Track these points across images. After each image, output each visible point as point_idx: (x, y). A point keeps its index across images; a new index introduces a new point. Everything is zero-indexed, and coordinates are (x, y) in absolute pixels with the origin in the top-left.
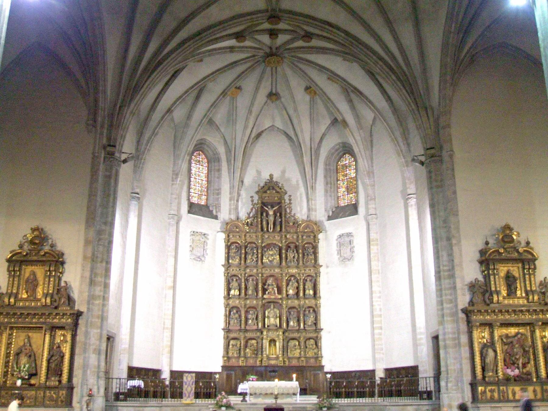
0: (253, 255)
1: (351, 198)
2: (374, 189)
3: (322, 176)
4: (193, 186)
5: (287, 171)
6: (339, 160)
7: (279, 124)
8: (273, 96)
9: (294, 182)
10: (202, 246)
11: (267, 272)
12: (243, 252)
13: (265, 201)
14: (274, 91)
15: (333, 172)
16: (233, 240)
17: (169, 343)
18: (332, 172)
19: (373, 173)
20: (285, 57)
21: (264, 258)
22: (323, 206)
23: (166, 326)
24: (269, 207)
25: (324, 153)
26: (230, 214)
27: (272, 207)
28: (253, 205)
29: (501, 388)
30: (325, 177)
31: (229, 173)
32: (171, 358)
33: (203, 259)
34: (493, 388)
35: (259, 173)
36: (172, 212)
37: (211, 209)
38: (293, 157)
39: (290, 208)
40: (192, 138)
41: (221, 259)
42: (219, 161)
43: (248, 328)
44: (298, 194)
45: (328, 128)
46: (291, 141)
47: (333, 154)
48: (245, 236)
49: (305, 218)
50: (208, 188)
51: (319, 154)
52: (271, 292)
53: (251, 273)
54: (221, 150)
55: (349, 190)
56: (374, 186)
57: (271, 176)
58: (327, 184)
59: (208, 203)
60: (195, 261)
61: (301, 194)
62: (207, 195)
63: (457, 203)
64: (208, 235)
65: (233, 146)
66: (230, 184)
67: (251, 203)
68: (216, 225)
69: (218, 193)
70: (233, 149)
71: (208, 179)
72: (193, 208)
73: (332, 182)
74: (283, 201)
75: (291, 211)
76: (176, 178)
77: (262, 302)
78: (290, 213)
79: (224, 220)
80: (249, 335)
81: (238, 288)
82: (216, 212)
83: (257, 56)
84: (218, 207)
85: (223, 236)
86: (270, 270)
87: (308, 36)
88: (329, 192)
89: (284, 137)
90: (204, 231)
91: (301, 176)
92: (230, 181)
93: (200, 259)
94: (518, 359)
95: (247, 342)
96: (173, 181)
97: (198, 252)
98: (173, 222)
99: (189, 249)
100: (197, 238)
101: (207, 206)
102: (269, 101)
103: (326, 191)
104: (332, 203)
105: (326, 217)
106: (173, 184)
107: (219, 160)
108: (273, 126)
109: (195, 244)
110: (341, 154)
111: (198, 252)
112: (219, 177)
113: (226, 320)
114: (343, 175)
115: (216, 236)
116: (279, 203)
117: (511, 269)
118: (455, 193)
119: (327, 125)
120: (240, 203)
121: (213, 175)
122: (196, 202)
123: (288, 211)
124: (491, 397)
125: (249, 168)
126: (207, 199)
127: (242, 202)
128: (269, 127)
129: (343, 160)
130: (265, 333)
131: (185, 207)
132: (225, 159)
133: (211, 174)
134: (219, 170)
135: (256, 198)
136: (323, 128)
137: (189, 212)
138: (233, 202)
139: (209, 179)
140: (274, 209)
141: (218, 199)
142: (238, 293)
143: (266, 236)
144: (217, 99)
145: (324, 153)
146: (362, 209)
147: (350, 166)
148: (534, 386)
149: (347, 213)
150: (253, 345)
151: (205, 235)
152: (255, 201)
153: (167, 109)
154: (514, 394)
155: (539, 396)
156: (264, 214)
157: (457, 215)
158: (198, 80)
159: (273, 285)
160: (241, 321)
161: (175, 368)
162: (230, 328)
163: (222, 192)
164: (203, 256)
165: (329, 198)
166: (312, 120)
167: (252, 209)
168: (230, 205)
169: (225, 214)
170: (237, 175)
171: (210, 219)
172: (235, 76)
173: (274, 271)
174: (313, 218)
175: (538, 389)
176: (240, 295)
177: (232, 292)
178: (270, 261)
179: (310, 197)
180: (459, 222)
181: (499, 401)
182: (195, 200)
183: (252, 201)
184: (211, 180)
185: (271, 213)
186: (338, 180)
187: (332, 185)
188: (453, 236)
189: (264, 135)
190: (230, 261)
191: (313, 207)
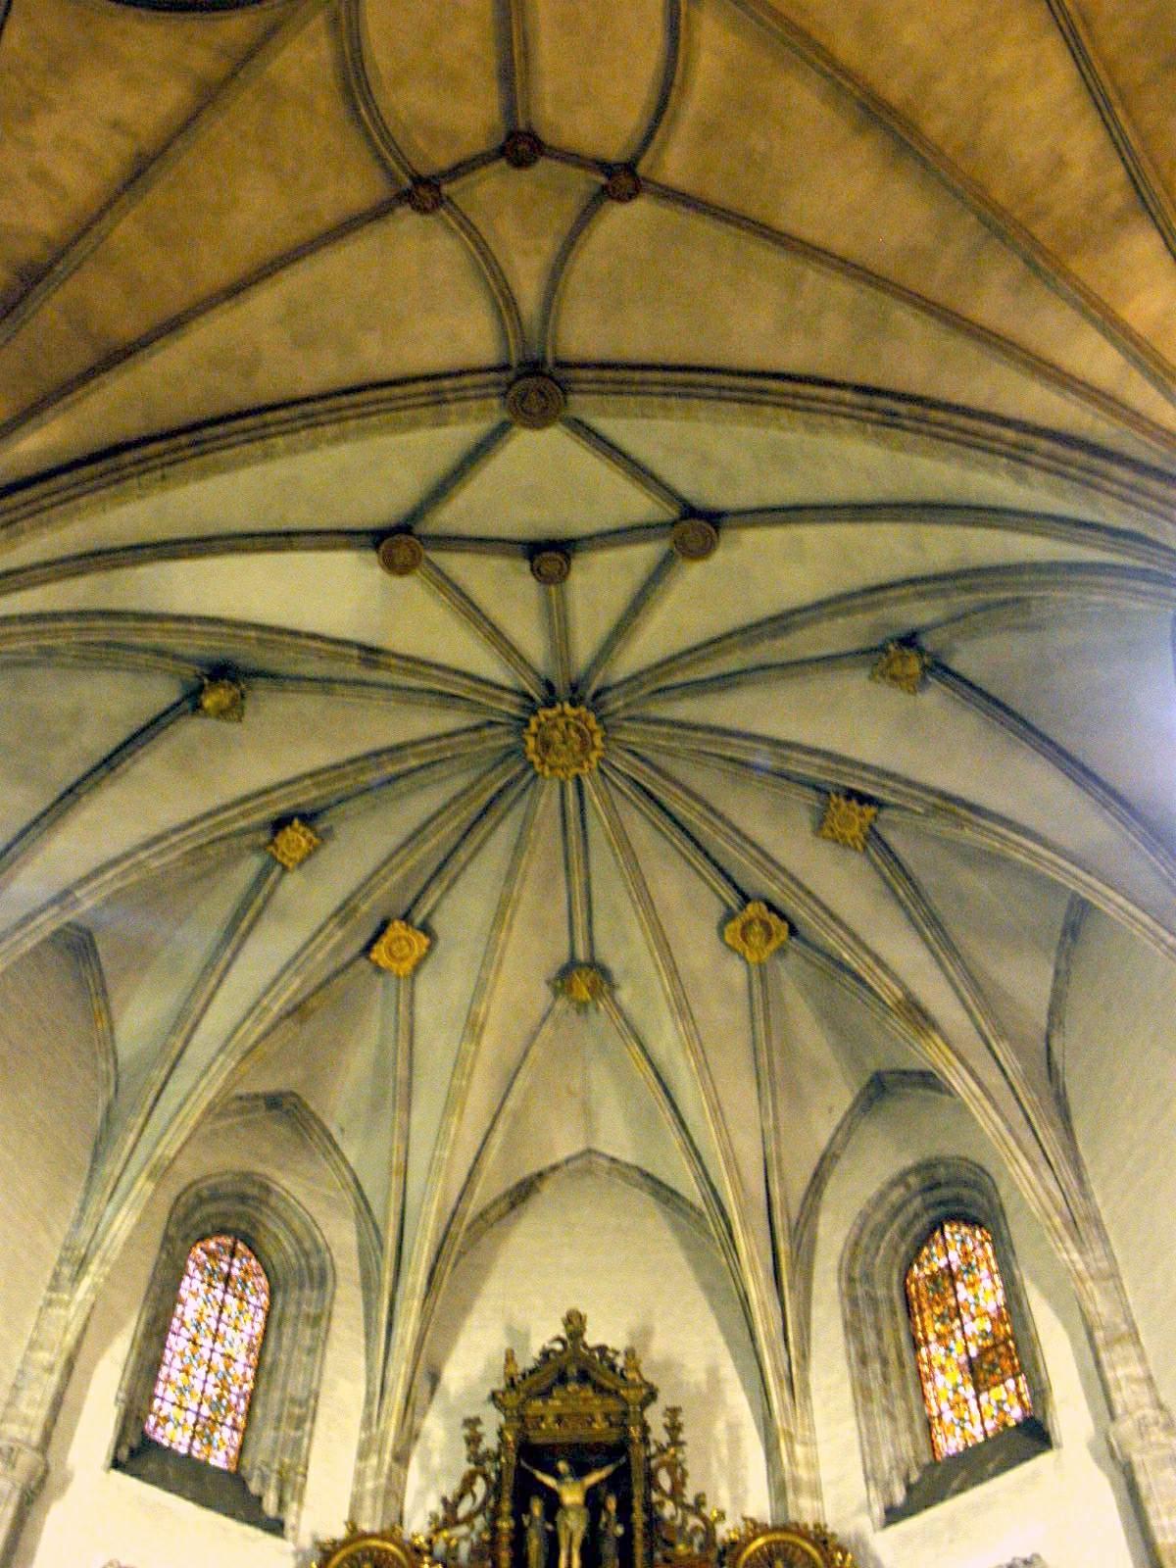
1: (1000, 1403)
2: (1120, 1288)
3: (845, 1396)
4: (176, 1376)
5: (658, 1328)
6: (913, 1258)
7: (617, 1139)
8: (582, 978)
9: (695, 1373)
13: (537, 1438)
14: (581, 954)
15: (895, 1311)
18: (884, 1309)
19: (1098, 1223)
22: (855, 1462)
24: (562, 1466)
25: (833, 1235)
27: (580, 1471)
28: (477, 1459)
30: (852, 1329)
31: (367, 1335)
37: (254, 1487)
38: (688, 1274)
39: (674, 1467)
40: (181, 1106)
42: (323, 1283)
44: (720, 1428)
45: (847, 1129)
46: (680, 1210)
47: (879, 1232)
49: (759, 1505)
50: (252, 1399)
51: (813, 1242)
54: (341, 1236)
55: (980, 1372)
56: (1114, 1275)
57: (575, 1323)
58: (863, 1360)
59: (246, 1461)
61: (733, 1428)
62: (245, 1432)
65: (394, 1206)
66: (369, 1381)
67: (463, 1450)
69: (303, 1413)
70: (393, 1220)
71: (260, 1359)
73: (892, 1356)
74: (635, 1432)
75: (678, 1486)
76: (75, 1279)
78: (676, 1494)
82: (281, 1504)
84: (291, 1483)
88: (877, 1394)
89: (643, 1200)
91: (731, 1343)
92: (370, 1369)
96: (53, 1288)
101: (236, 1478)
103: (863, 1393)
104: (898, 1447)
105: (878, 1511)
106: (49, 1303)
107: (320, 1278)
108: (590, 1151)
110: (917, 1228)
112: (317, 1349)
114: (941, 1318)
116: (616, 1451)
119: (838, 1116)
120: (414, 1477)
121: (285, 1342)
122: (183, 1450)
123: (665, 1481)
125: (472, 1321)
126: (241, 1450)
128: (568, 1161)
129: (929, 1259)
132: (357, 1276)
133: (279, 1339)
134: (319, 1321)
135: (492, 1422)
136: (823, 1130)
138: (373, 1461)
140: (593, 1478)
144: (312, 939)
145: (833, 1235)
146: (1071, 1415)
147: (970, 1269)
149: (991, 1467)
152: (490, 1442)
156: (537, 1507)
163: (324, 1412)
165: (883, 1425)
166: (766, 1079)
167: (468, 1483)
168: (360, 1477)
170: (408, 1328)
172: (392, 840)
174: (805, 1510)
179: (779, 1422)
182: (175, 1436)
183: (473, 1440)
184: (275, 1363)
185: (572, 1495)
186: (916, 1346)
187: (890, 1364)
189: (547, 1189)
191: (803, 1473)
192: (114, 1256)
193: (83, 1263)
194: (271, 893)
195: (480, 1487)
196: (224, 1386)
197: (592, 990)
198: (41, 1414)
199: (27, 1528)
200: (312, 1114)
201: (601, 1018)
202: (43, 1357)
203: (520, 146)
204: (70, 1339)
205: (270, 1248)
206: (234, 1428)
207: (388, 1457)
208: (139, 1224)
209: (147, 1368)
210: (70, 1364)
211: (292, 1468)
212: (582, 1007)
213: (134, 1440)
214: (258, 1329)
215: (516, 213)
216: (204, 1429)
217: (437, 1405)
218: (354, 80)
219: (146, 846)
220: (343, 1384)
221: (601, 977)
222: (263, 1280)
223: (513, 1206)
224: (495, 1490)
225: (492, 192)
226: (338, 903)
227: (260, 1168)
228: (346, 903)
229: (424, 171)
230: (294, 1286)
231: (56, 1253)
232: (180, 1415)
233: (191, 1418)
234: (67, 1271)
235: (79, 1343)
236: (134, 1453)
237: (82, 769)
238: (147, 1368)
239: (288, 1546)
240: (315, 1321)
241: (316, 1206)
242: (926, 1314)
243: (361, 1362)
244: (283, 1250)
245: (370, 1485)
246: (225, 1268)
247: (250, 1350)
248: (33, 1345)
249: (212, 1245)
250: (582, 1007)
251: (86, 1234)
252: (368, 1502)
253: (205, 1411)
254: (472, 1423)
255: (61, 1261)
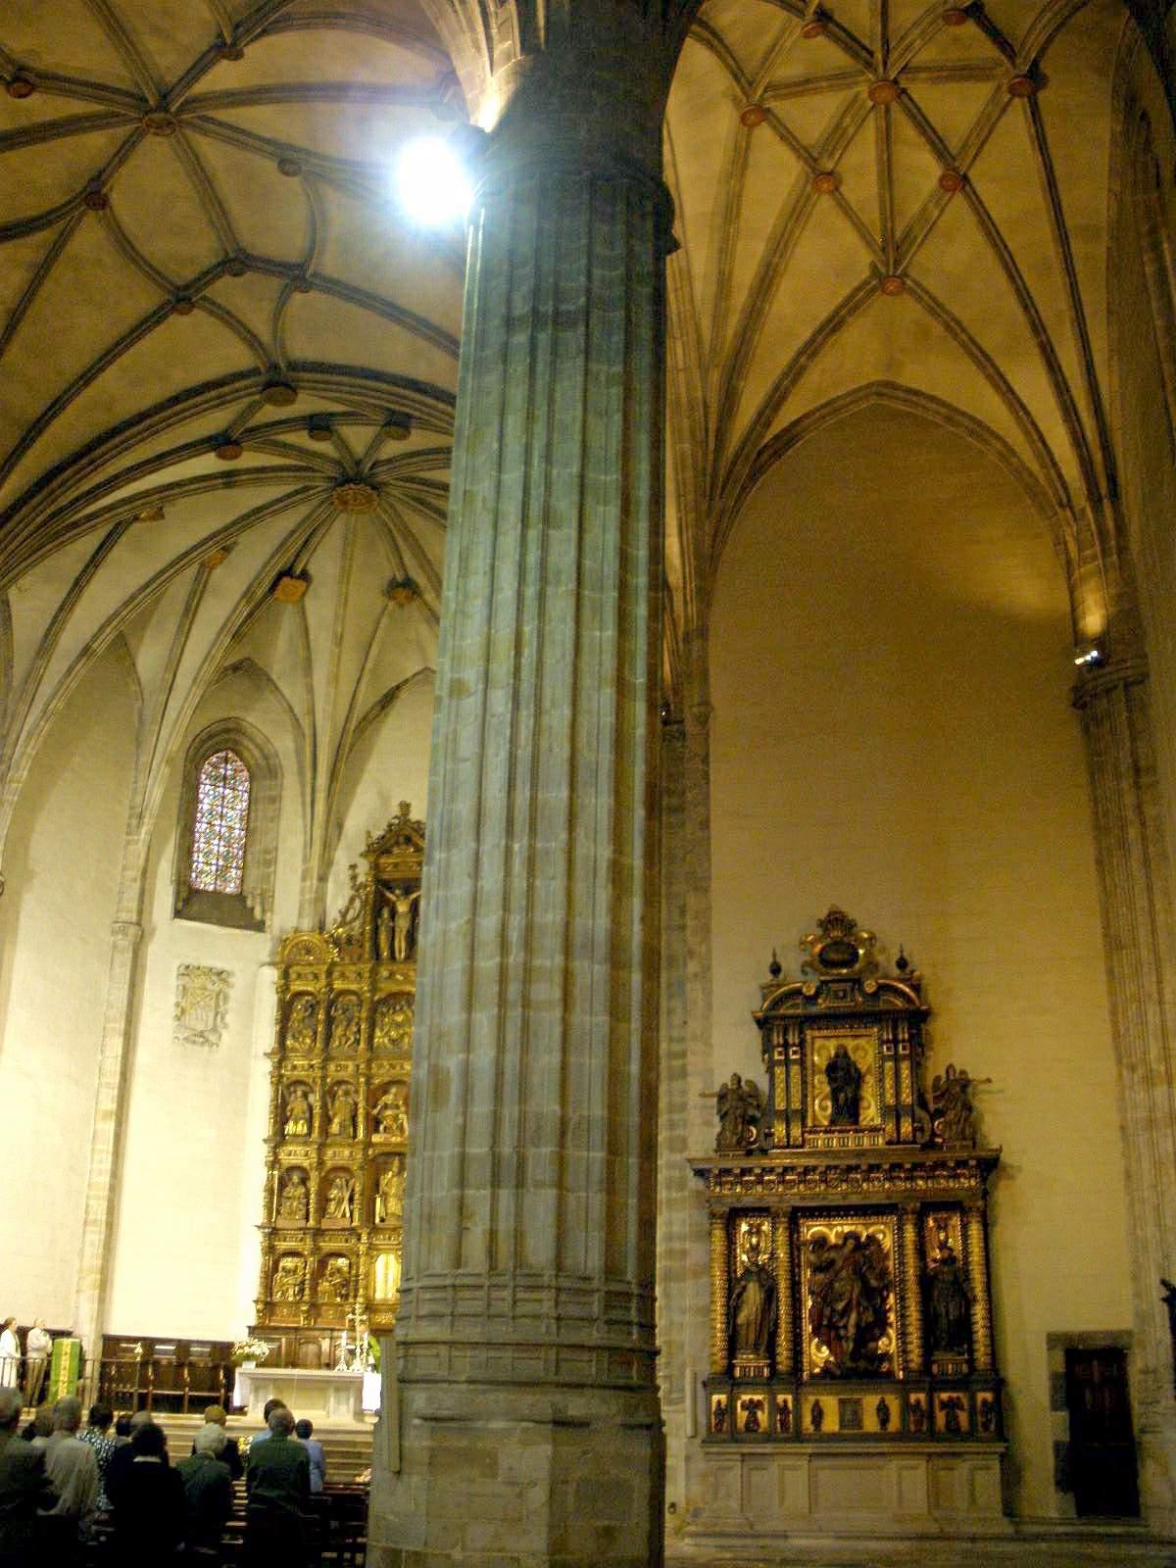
0: (348, 1025)
10: (213, 1003)
11: (382, 1073)
12: (321, 1016)
13: (385, 876)
16: (297, 986)
17: (99, 1262)
20: (386, 484)
21: (378, 1033)
23: (91, 1217)
26: (300, 915)
28: (357, 888)
29: (780, 1398)
32: (103, 1300)
33: (213, 1038)
34: (757, 1397)
35: (384, 799)
36: (124, 916)
37: (249, 903)
41: (266, 1036)
43: (325, 1224)
48: (329, 973)
50: (245, 848)
52: (391, 1127)
53: (342, 1075)
54: (284, 745)
60: (188, 1045)
63: (708, 853)
64: (229, 974)
68: (259, 946)
69: (269, 860)
72: (190, 902)
76: (139, 826)
77: (365, 1154)
79: (282, 931)
80: (327, 1245)
81: (307, 1115)
82: (264, 911)
83: (313, 488)
84: (267, 899)
85: (271, 975)
86: (393, 1067)
87: (396, 424)
90: (219, 965)
93: (202, 1038)
94: (845, 1312)
95: (323, 1263)
97: (200, 1020)
98: (125, 943)
99: (173, 1011)
100: (199, 982)
101: (240, 897)
102: (391, 604)
106: (128, 843)
109: (190, 998)
111: (200, 1020)
112: (276, 818)
113: (271, 1202)
115: (255, 976)
117: (850, 1044)
118: (705, 825)
120: (330, 885)
124: (747, 1424)
125: (360, 789)
127: (336, 882)
128: (414, 676)
130: (364, 1238)
131: (164, 897)
134: (275, 800)
137: (178, 914)
138: (308, 883)
139: (252, 825)
141: (266, 878)
142: (305, 1131)
143: (385, 974)
148: (883, 1392)
150: (339, 1270)
151: (219, 974)
153: (81, 646)
154: (818, 1416)
155: (894, 1424)
156: (386, 913)
157: (706, 890)
158: (159, 567)
159: (397, 1107)
160: (308, 1204)
161: (116, 1329)
162: (281, 1224)
164: (215, 1029)
167: (352, 900)
168: (302, 892)
169: (287, 912)
171: (237, 931)
173: (402, 1068)
175: (894, 1404)
176: (309, 1134)
177: (290, 1128)
178: (393, 1041)
180: (709, 908)
181: (769, 1437)
182: (206, 882)
183: (354, 878)
188: (691, 953)
189: (403, 695)
190: (289, 1043)
192: (155, 812)
193: (141, 817)
194: (206, 581)
195: (357, 904)
196: (229, 845)
197: (407, 597)
198: (134, 905)
199: (139, 970)
200: (261, 669)
201: (415, 604)
202: (130, 874)
203: (237, 262)
204: (141, 862)
205: (246, 754)
206: (237, 868)
207: (315, 882)
208: (166, 790)
209: (186, 852)
210: (144, 872)
211: (267, 891)
212: (401, 606)
213: (184, 895)
214: (245, 804)
215: (243, 295)
216: (221, 873)
217: (342, 845)
218: (125, 245)
219: (126, 604)
220: (292, 836)
221: (408, 584)
222: (246, 774)
223: (383, 708)
224: (364, 904)
225: (226, 290)
226: (244, 588)
227: (233, 714)
228: (248, 589)
229: (180, 283)
230: (263, 773)
231: (127, 813)
232: (207, 868)
233: (214, 868)
234: (134, 822)
235: (147, 860)
236: (187, 901)
237: (80, 567)
238: (186, 852)
239: (268, 936)
240: (273, 800)
241: (264, 723)
242: (452, 1063)
243: (300, 822)
244: (253, 756)
245: (307, 897)
246: (222, 771)
247: (241, 820)
248: (124, 868)
249: (214, 759)
250: (401, 606)
251: (139, 799)
252: (306, 906)
253: (221, 863)
254: (353, 867)
255: (131, 817)
